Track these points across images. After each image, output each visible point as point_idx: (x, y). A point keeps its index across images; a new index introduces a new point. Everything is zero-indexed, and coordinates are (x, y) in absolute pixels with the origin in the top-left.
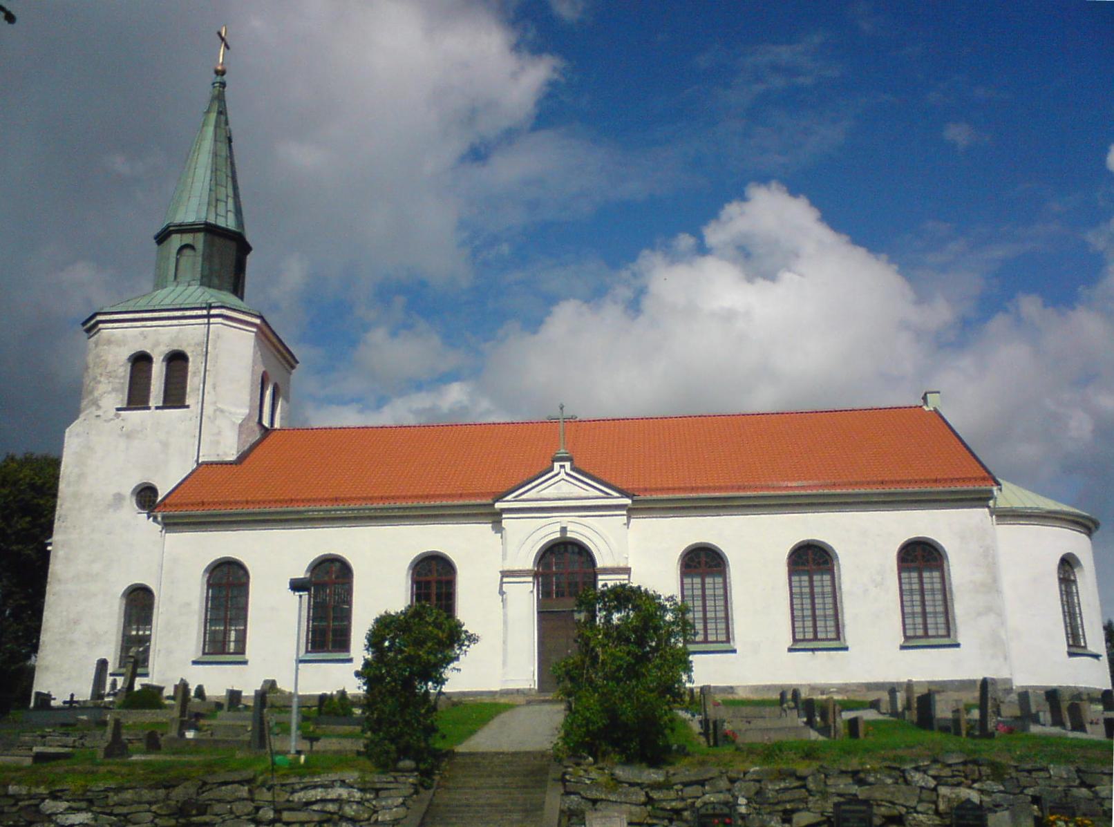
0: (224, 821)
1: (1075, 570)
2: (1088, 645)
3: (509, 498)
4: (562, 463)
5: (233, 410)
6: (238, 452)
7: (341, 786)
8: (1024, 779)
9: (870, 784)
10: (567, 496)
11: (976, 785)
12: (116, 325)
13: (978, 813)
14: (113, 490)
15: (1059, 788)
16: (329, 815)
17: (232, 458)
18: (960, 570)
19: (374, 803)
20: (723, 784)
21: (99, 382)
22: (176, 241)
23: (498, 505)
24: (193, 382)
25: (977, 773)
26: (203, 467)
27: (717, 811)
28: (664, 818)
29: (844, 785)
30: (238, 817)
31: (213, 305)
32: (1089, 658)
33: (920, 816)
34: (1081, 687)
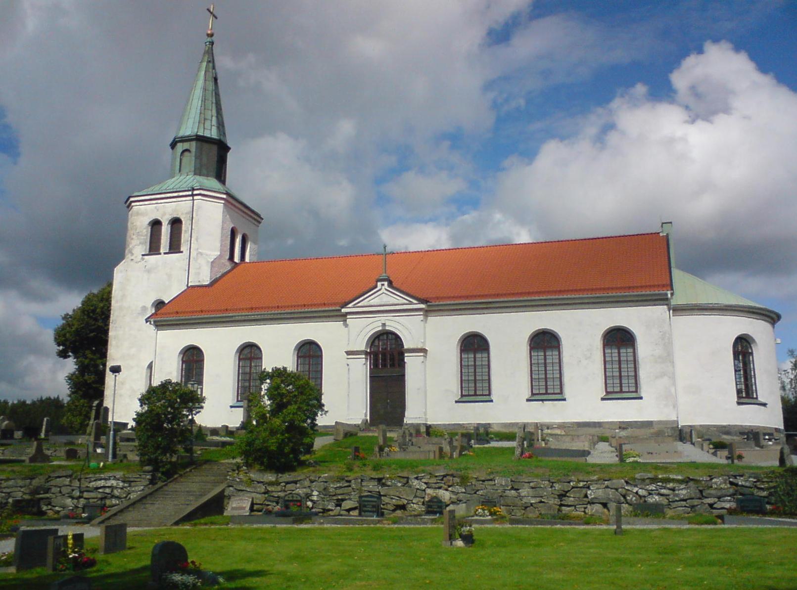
0: (57, 496)
1: (752, 345)
2: (759, 397)
3: (350, 305)
4: (383, 283)
5: (209, 253)
6: (211, 279)
7: (113, 480)
8: (479, 485)
9: (389, 486)
10: (386, 303)
11: (450, 489)
12: (141, 203)
13: (440, 504)
14: (141, 304)
15: (499, 491)
16: (106, 495)
17: (207, 283)
18: (644, 348)
19: (128, 488)
20: (307, 483)
21: (132, 239)
22: (180, 147)
23: (344, 310)
24: (185, 236)
25: (451, 481)
26: (190, 288)
27: (295, 499)
28: (273, 502)
29: (372, 486)
30: (64, 495)
31: (195, 188)
32: (757, 406)
33: (415, 505)
34: (746, 426)
